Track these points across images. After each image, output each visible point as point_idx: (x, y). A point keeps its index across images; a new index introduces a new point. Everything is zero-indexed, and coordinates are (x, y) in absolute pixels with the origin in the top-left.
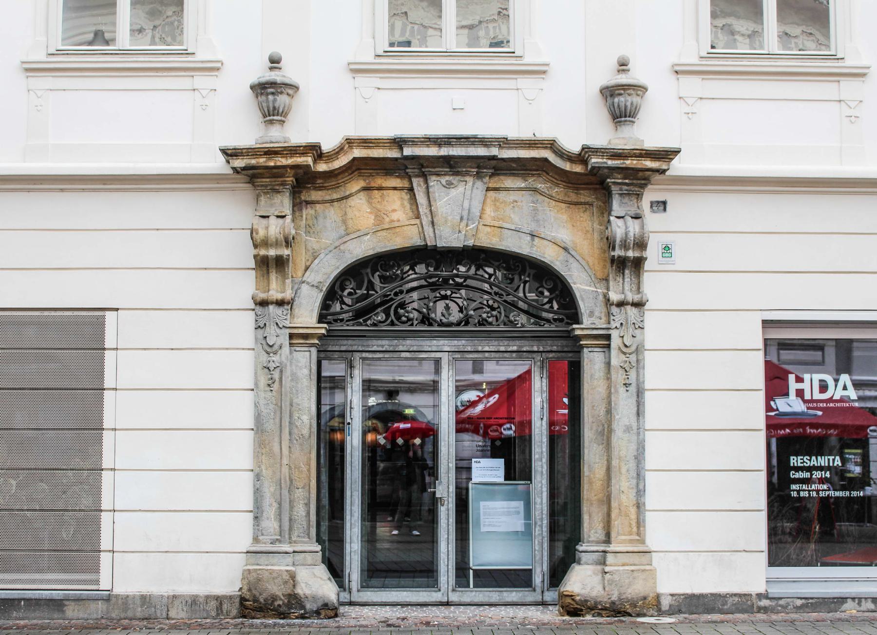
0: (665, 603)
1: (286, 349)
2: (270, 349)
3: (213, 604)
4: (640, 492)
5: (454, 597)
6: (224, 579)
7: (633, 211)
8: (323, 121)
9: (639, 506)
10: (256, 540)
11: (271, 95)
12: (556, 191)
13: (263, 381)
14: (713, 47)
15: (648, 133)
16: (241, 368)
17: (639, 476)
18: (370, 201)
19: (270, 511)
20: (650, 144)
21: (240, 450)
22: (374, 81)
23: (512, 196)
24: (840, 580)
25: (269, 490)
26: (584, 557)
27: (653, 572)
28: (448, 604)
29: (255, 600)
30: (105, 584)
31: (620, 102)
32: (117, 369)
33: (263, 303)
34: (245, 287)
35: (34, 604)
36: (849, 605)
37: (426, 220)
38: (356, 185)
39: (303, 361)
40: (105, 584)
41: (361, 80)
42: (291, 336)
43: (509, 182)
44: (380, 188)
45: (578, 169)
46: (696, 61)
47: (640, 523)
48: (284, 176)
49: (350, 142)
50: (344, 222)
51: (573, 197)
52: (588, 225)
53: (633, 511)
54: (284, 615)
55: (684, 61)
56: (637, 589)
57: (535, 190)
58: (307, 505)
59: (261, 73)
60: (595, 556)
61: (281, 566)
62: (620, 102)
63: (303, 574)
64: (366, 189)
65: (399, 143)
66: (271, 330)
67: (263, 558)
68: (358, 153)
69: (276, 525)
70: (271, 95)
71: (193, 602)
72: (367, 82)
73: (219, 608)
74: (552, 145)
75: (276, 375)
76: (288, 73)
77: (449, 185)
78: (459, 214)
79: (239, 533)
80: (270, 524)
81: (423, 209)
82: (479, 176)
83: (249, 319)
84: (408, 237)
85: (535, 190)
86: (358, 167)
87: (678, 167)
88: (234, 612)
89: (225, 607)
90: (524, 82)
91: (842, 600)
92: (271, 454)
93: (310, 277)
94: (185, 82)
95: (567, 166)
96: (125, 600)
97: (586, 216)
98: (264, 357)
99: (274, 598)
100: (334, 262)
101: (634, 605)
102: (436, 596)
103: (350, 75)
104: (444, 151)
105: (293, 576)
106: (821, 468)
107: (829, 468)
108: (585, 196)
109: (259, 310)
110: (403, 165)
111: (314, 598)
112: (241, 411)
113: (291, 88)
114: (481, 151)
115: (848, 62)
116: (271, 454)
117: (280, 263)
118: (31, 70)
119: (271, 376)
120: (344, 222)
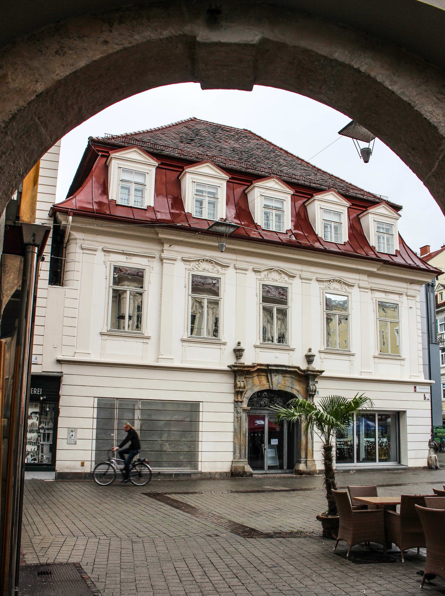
0: (317, 472)
1: (242, 413)
2: (238, 413)
3: (225, 474)
4: (313, 447)
5: (268, 472)
6: (226, 468)
7: (313, 384)
8: (248, 360)
9: (312, 450)
10: (234, 458)
11: (238, 352)
12: (296, 378)
13: (236, 420)
14: (381, 351)
15: (316, 366)
16: (230, 417)
17: (312, 443)
18: (258, 377)
19: (238, 452)
20: (317, 369)
21: (230, 437)
22: (106, 337)
23: (287, 379)
24: (351, 466)
25: (237, 447)
26: (302, 462)
27: (316, 465)
28: (266, 474)
29: (235, 473)
30: (199, 470)
31: (309, 359)
32: (203, 416)
33: (237, 402)
34: (231, 398)
35: (184, 474)
36: (351, 472)
37: (270, 383)
38: (256, 374)
39: (244, 416)
40: (199, 470)
41: (257, 349)
42: (243, 410)
43: (287, 375)
44: (261, 375)
45: (303, 373)
46: (106, 332)
47: (313, 454)
48: (239, 372)
49: (258, 365)
50: (253, 383)
51: (299, 379)
52: (302, 386)
53: (311, 451)
54: (242, 476)
55: (103, 331)
56: (313, 469)
57: (292, 377)
58: (245, 450)
59: (306, 352)
60: (304, 461)
61: (241, 465)
62: (309, 359)
63: (246, 466)
64: (257, 375)
65: (268, 366)
66: (239, 408)
67: (237, 463)
68: (259, 367)
69: (239, 455)
70: (238, 352)
71: (221, 474)
72: (186, 344)
73: (227, 475)
74: (298, 368)
75: (239, 419)
76: (242, 346)
77: (276, 376)
78: (279, 382)
79: (230, 457)
80: (238, 454)
81: (270, 381)
82: (282, 374)
83: (232, 405)
84: (266, 387)
85: (292, 377)
86: (259, 371)
87: (324, 374)
88: (230, 476)
89: (228, 475)
90: (290, 352)
91: (350, 470)
92: (238, 438)
93: (246, 396)
94: (218, 347)
95: (300, 373)
96: (205, 474)
97: (302, 384)
98: (236, 415)
99: (240, 472)
100: (251, 392)
101: (312, 472)
102: (264, 472)
103: (181, 342)
104: (277, 368)
105: (244, 466)
106: (342, 441)
107: (344, 441)
108: (302, 379)
109: (236, 403)
110: (267, 370)
111: (249, 472)
112: (230, 427)
113: (242, 350)
114: (284, 369)
115: (352, 352)
116: (238, 438)
117: (241, 393)
118: (102, 334)
119: (238, 419)
120: (253, 383)
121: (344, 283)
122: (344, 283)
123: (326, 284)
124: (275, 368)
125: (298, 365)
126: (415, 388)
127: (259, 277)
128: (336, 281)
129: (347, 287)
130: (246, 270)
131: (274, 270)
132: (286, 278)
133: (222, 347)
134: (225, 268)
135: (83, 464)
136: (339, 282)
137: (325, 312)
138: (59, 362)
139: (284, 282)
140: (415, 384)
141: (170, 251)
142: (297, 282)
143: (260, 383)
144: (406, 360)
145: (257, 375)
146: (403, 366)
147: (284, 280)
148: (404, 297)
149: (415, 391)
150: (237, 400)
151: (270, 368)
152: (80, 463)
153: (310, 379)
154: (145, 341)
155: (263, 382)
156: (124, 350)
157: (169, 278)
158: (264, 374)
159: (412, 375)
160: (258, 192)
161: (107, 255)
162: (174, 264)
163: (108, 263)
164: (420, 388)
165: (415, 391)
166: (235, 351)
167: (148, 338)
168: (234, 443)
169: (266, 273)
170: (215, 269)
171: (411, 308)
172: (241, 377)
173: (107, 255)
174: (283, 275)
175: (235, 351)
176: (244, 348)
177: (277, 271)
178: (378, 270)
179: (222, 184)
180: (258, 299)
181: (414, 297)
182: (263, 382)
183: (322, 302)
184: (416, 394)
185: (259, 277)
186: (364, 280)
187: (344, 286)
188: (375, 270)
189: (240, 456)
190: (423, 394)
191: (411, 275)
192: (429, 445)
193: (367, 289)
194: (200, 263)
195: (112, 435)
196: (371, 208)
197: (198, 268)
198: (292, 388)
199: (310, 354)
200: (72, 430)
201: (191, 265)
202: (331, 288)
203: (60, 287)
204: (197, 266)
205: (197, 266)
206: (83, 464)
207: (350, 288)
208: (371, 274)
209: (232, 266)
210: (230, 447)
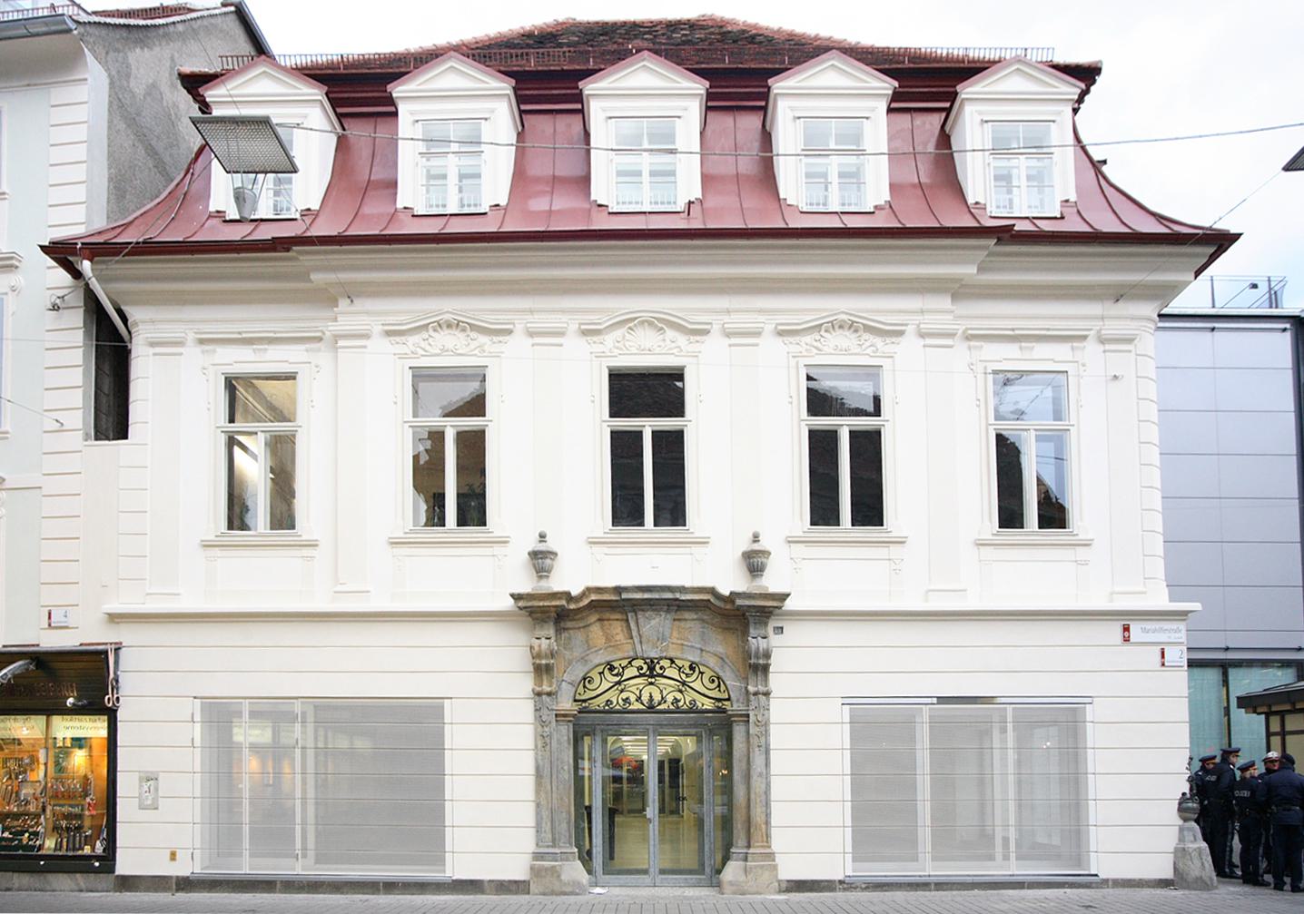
4: (768, 815)
8: (571, 578)
9: (767, 823)
11: (541, 560)
15: (772, 582)
18: (602, 627)
20: (773, 589)
22: (217, 552)
23: (689, 624)
25: (546, 814)
31: (754, 563)
34: (527, 684)
38: (593, 618)
41: (596, 548)
43: (687, 615)
44: (608, 620)
46: (991, 537)
48: (550, 614)
50: (587, 642)
59: (746, 545)
62: (754, 563)
64: (599, 620)
66: (545, 711)
68: (594, 597)
70: (541, 560)
74: (712, 591)
75: (548, 741)
81: (635, 633)
85: (703, 621)
86: (593, 606)
87: (789, 605)
90: (696, 549)
95: (718, 603)
98: (540, 729)
112: (527, 763)
113: (766, 553)
121: (868, 329)
122: (868, 329)
123: (808, 339)
124: (638, 596)
125: (708, 584)
126: (1126, 629)
127: (598, 348)
128: (449, 326)
129: (878, 341)
130: (561, 334)
131: (642, 323)
132: (682, 340)
133: (497, 549)
134: (894, 340)
135: (173, 856)
136: (852, 326)
137: (991, 428)
138: (114, 618)
139: (675, 351)
140: (1126, 621)
141: (349, 317)
142: (714, 345)
143: (608, 639)
144: (908, 540)
145: (599, 620)
146: (1086, 563)
147: (673, 345)
148: (1091, 349)
149: (1127, 640)
150: (538, 689)
151: (624, 596)
152: (168, 852)
153: (751, 619)
154: (306, 552)
155: (618, 638)
156: (260, 575)
157: (356, 387)
158: (618, 616)
159: (1117, 589)
160: (788, 111)
161: (1078, 348)
162: (757, 345)
163: (980, 368)
164: (1145, 631)
165: (1127, 640)
166: (535, 555)
167: (314, 545)
168: (538, 805)
169: (619, 333)
170: (474, 345)
171: (1115, 377)
172: (546, 626)
173: (1078, 348)
174: (670, 333)
175: (535, 555)
176: (768, 548)
177: (651, 324)
178: (981, 269)
179: (1059, 113)
180: (983, 413)
181: (1130, 340)
182: (618, 638)
183: (794, 395)
184: (1127, 648)
185: (598, 348)
186: (940, 312)
187: (866, 336)
188: (968, 270)
189: (554, 840)
190: (1157, 650)
191: (1088, 270)
192: (1180, 809)
193: (951, 335)
194: (823, 333)
195: (240, 786)
196: (399, 85)
197: (428, 348)
198: (702, 650)
199: (542, 547)
200: (151, 778)
201: (410, 344)
202: (825, 348)
203: (107, 442)
204: (423, 344)
205: (423, 344)
206: (173, 856)
207: (888, 340)
208: (960, 291)
209: (910, 329)
210: (527, 815)
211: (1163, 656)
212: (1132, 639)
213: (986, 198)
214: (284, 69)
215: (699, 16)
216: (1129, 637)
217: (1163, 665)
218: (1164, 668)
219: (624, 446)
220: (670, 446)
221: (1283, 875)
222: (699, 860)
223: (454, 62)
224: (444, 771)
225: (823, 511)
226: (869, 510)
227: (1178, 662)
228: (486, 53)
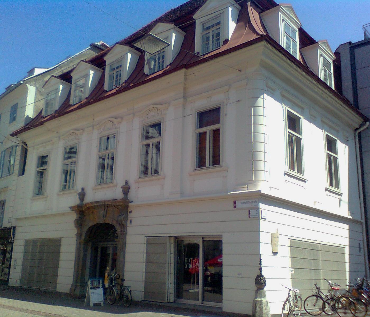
11: (82, 195)
70: (82, 195)
149: (235, 207)
165: (235, 207)
211: (249, 214)
212: (237, 207)
213: (262, 33)
214: (53, 117)
215: (89, 93)
216: (236, 206)
217: (249, 217)
218: (250, 219)
219: (201, 138)
220: (216, 134)
221: (210, 282)
222: (253, 306)
223: (160, 24)
224: (292, 281)
225: (201, 163)
226: (216, 161)
227: (255, 216)
228: (165, 19)
